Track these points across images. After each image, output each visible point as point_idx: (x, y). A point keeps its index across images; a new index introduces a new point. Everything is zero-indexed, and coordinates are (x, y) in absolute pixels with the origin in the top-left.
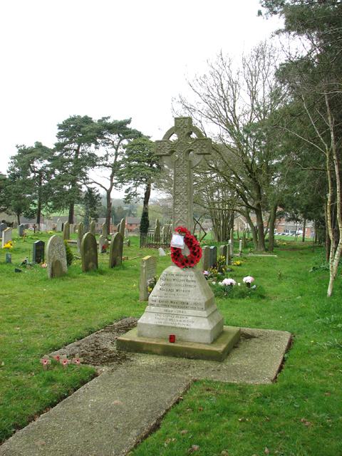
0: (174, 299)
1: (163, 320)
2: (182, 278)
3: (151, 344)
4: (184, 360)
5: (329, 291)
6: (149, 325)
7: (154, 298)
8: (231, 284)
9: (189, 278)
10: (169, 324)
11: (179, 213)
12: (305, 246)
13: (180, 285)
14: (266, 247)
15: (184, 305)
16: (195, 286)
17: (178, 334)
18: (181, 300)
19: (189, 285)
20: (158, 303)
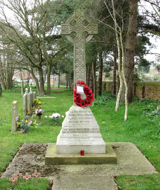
0: (79, 127)
1: (73, 142)
2: (84, 113)
3: (70, 158)
4: (93, 166)
5: (126, 117)
6: (64, 146)
7: (66, 128)
8: (58, 116)
9: (88, 113)
10: (78, 143)
11: (78, 72)
12: (60, 90)
13: (82, 118)
14: (46, 92)
15: (86, 131)
16: (93, 118)
17: (86, 150)
18: (84, 127)
19: (87, 117)
20: (69, 131)
